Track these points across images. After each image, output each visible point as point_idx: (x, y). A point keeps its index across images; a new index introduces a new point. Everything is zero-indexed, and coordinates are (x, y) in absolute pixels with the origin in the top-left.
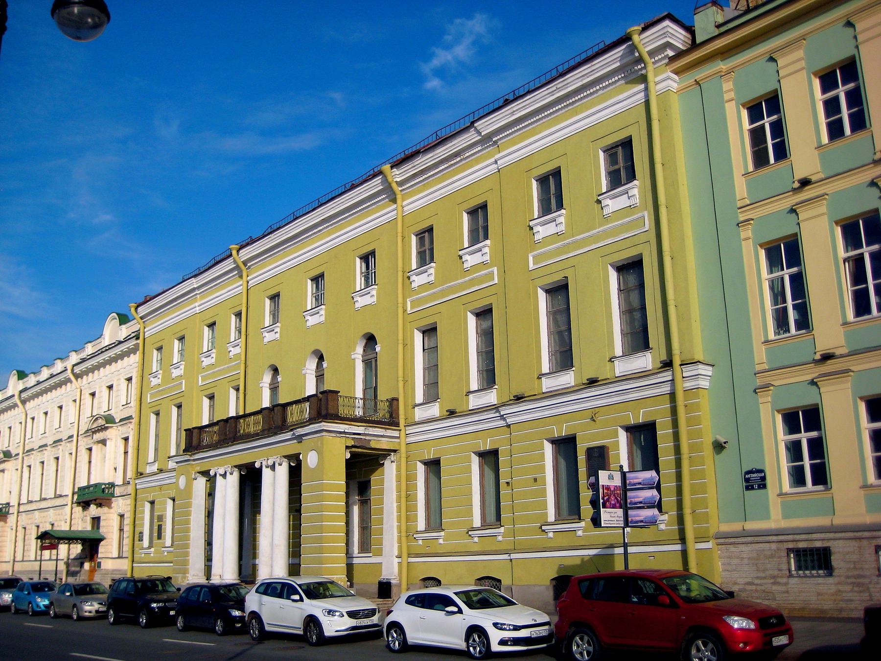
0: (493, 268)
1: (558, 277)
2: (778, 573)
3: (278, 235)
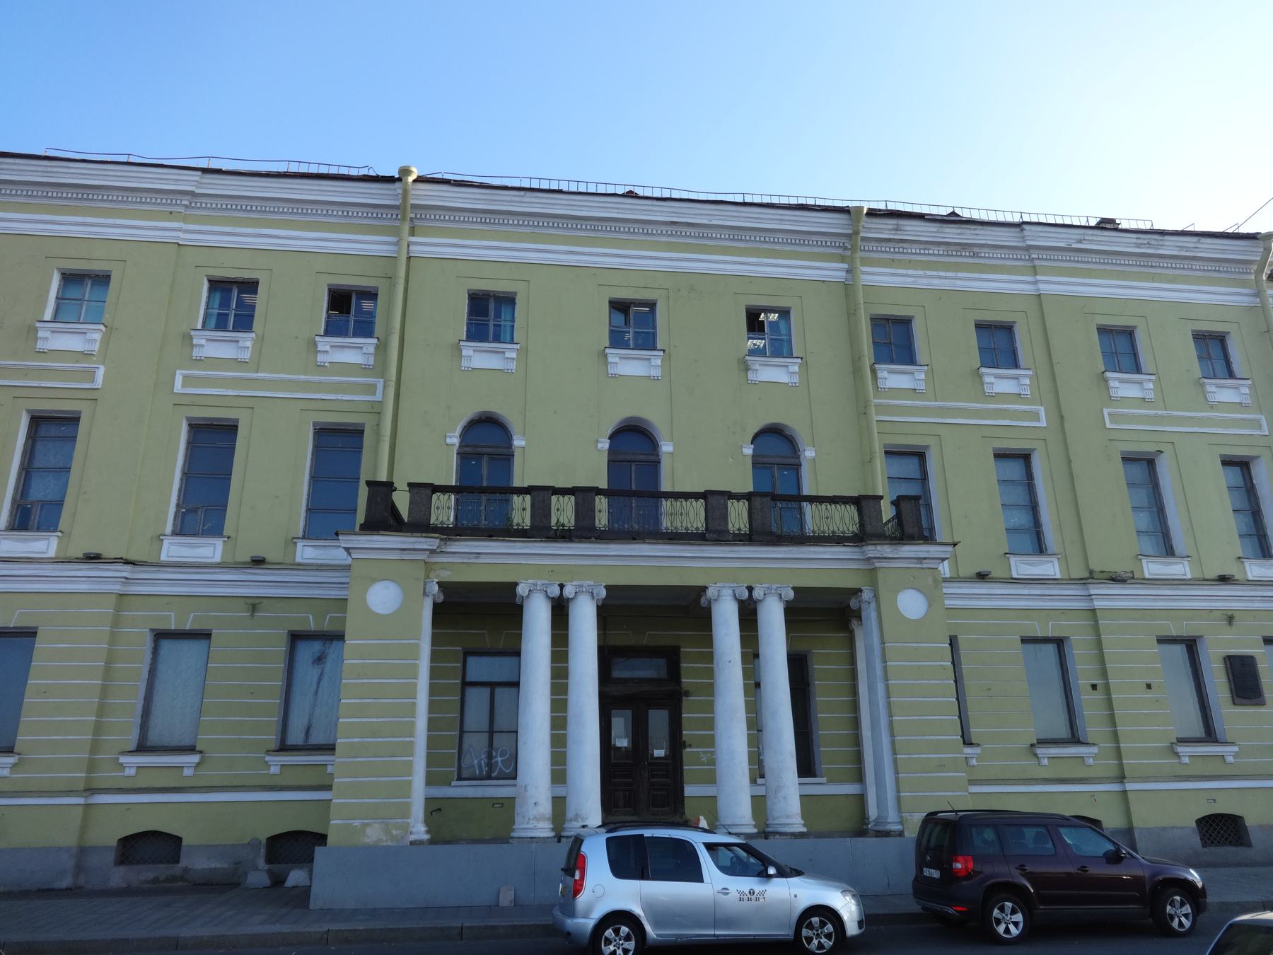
0: (1041, 407)
3: (544, 201)
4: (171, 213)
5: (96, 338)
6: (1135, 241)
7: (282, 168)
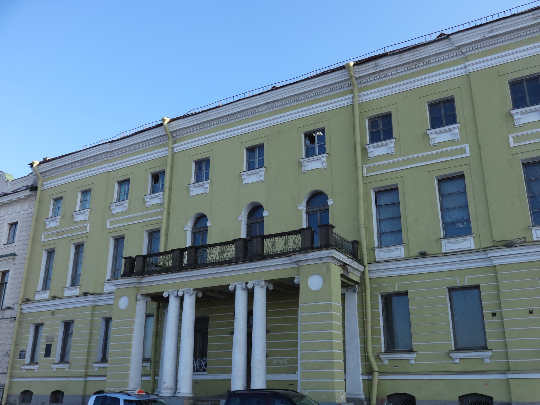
0: (466, 145)
3: (215, 113)
4: (106, 160)
5: (263, 174)
6: (531, 17)
7: (142, 129)
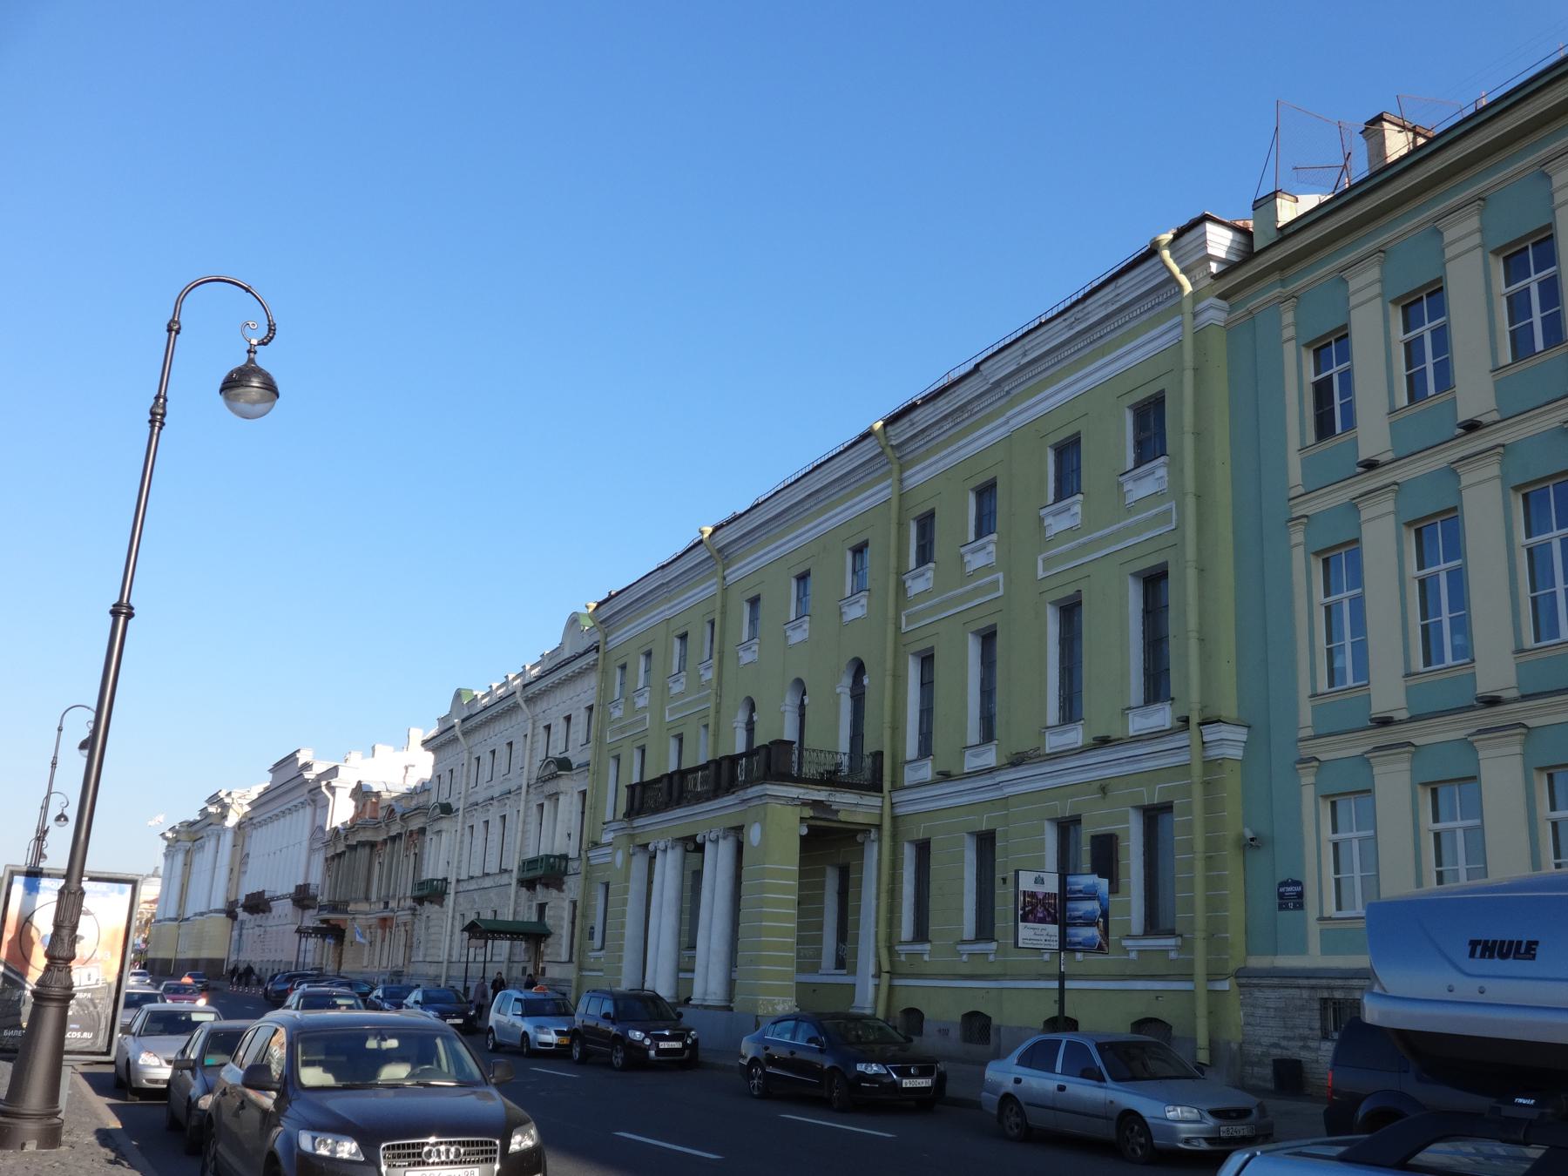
1: (1070, 591)
2: (1309, 1032)
